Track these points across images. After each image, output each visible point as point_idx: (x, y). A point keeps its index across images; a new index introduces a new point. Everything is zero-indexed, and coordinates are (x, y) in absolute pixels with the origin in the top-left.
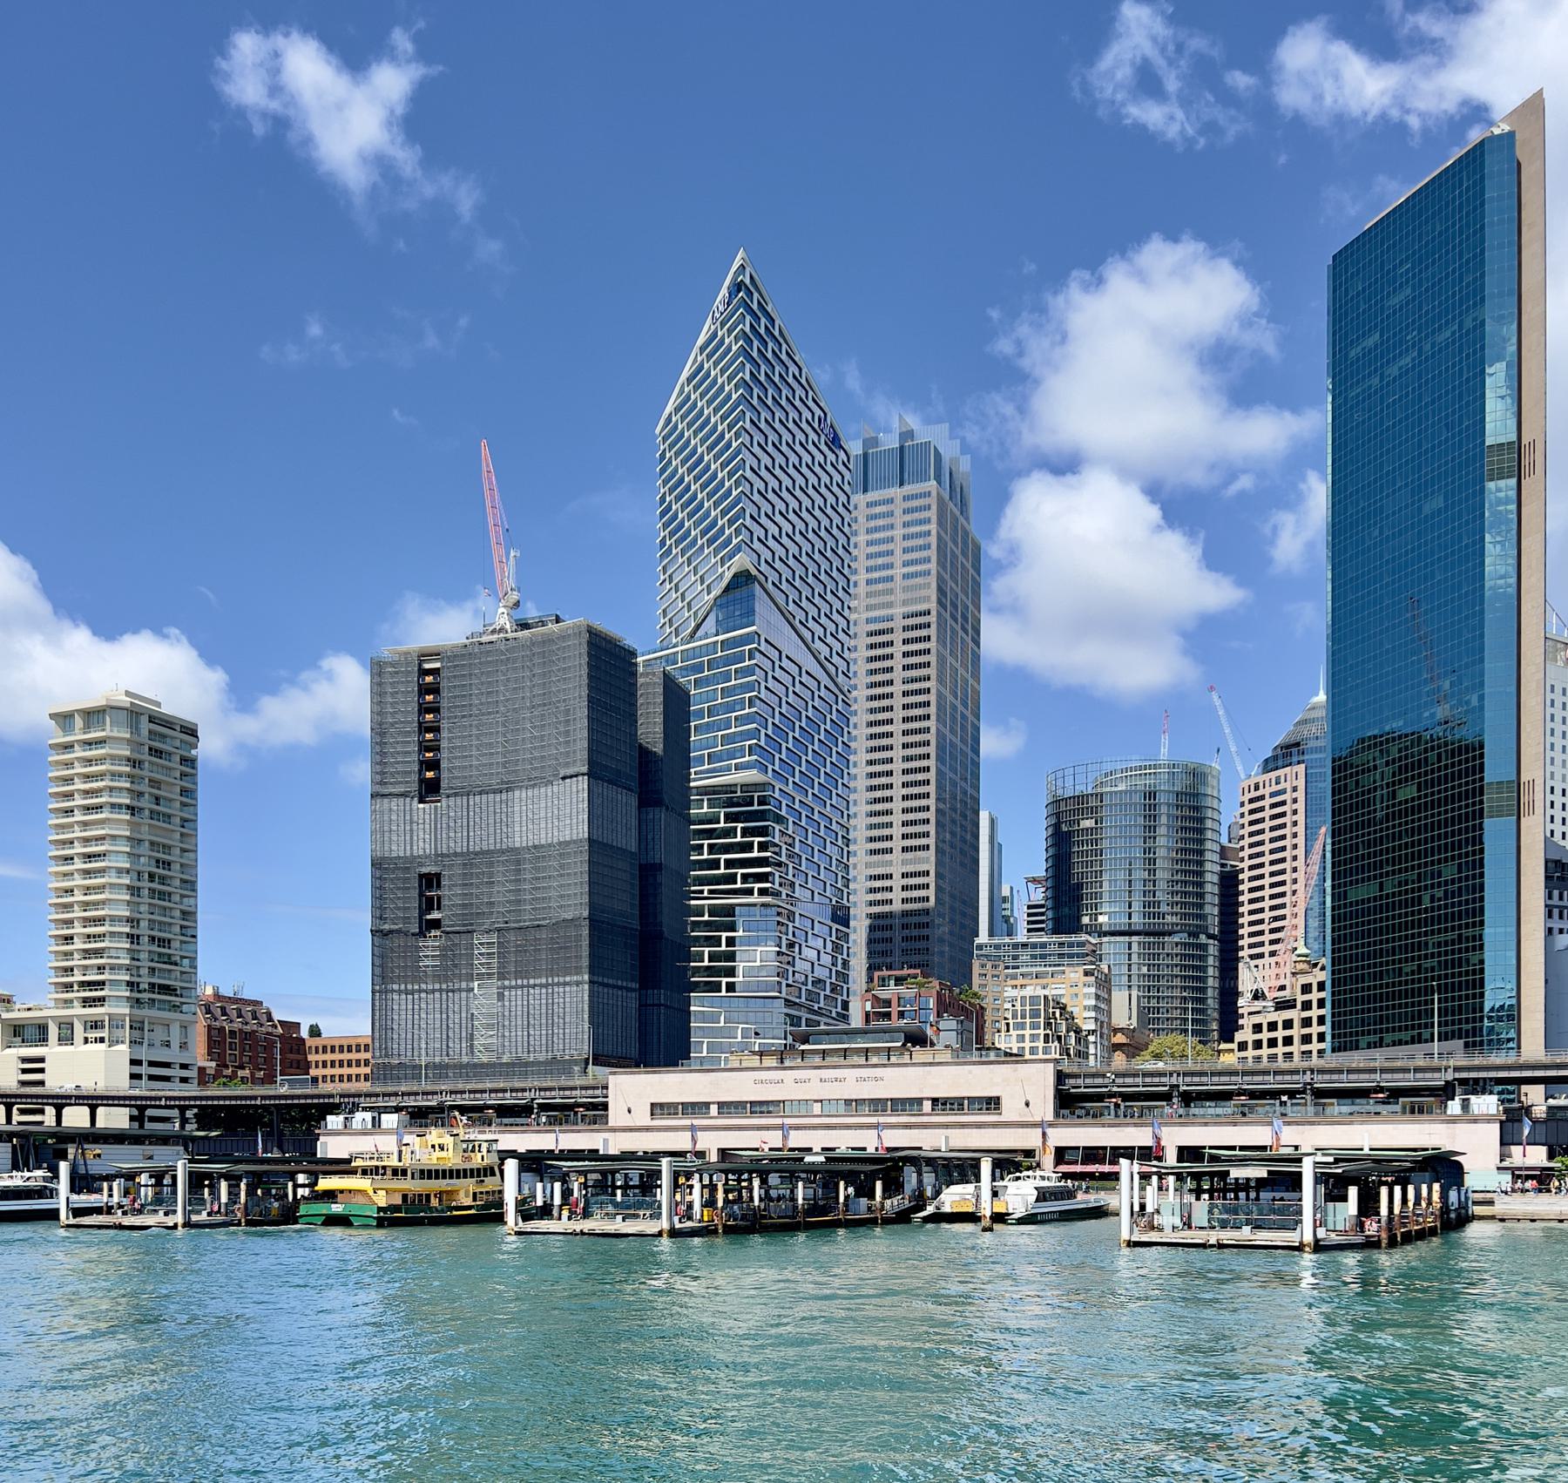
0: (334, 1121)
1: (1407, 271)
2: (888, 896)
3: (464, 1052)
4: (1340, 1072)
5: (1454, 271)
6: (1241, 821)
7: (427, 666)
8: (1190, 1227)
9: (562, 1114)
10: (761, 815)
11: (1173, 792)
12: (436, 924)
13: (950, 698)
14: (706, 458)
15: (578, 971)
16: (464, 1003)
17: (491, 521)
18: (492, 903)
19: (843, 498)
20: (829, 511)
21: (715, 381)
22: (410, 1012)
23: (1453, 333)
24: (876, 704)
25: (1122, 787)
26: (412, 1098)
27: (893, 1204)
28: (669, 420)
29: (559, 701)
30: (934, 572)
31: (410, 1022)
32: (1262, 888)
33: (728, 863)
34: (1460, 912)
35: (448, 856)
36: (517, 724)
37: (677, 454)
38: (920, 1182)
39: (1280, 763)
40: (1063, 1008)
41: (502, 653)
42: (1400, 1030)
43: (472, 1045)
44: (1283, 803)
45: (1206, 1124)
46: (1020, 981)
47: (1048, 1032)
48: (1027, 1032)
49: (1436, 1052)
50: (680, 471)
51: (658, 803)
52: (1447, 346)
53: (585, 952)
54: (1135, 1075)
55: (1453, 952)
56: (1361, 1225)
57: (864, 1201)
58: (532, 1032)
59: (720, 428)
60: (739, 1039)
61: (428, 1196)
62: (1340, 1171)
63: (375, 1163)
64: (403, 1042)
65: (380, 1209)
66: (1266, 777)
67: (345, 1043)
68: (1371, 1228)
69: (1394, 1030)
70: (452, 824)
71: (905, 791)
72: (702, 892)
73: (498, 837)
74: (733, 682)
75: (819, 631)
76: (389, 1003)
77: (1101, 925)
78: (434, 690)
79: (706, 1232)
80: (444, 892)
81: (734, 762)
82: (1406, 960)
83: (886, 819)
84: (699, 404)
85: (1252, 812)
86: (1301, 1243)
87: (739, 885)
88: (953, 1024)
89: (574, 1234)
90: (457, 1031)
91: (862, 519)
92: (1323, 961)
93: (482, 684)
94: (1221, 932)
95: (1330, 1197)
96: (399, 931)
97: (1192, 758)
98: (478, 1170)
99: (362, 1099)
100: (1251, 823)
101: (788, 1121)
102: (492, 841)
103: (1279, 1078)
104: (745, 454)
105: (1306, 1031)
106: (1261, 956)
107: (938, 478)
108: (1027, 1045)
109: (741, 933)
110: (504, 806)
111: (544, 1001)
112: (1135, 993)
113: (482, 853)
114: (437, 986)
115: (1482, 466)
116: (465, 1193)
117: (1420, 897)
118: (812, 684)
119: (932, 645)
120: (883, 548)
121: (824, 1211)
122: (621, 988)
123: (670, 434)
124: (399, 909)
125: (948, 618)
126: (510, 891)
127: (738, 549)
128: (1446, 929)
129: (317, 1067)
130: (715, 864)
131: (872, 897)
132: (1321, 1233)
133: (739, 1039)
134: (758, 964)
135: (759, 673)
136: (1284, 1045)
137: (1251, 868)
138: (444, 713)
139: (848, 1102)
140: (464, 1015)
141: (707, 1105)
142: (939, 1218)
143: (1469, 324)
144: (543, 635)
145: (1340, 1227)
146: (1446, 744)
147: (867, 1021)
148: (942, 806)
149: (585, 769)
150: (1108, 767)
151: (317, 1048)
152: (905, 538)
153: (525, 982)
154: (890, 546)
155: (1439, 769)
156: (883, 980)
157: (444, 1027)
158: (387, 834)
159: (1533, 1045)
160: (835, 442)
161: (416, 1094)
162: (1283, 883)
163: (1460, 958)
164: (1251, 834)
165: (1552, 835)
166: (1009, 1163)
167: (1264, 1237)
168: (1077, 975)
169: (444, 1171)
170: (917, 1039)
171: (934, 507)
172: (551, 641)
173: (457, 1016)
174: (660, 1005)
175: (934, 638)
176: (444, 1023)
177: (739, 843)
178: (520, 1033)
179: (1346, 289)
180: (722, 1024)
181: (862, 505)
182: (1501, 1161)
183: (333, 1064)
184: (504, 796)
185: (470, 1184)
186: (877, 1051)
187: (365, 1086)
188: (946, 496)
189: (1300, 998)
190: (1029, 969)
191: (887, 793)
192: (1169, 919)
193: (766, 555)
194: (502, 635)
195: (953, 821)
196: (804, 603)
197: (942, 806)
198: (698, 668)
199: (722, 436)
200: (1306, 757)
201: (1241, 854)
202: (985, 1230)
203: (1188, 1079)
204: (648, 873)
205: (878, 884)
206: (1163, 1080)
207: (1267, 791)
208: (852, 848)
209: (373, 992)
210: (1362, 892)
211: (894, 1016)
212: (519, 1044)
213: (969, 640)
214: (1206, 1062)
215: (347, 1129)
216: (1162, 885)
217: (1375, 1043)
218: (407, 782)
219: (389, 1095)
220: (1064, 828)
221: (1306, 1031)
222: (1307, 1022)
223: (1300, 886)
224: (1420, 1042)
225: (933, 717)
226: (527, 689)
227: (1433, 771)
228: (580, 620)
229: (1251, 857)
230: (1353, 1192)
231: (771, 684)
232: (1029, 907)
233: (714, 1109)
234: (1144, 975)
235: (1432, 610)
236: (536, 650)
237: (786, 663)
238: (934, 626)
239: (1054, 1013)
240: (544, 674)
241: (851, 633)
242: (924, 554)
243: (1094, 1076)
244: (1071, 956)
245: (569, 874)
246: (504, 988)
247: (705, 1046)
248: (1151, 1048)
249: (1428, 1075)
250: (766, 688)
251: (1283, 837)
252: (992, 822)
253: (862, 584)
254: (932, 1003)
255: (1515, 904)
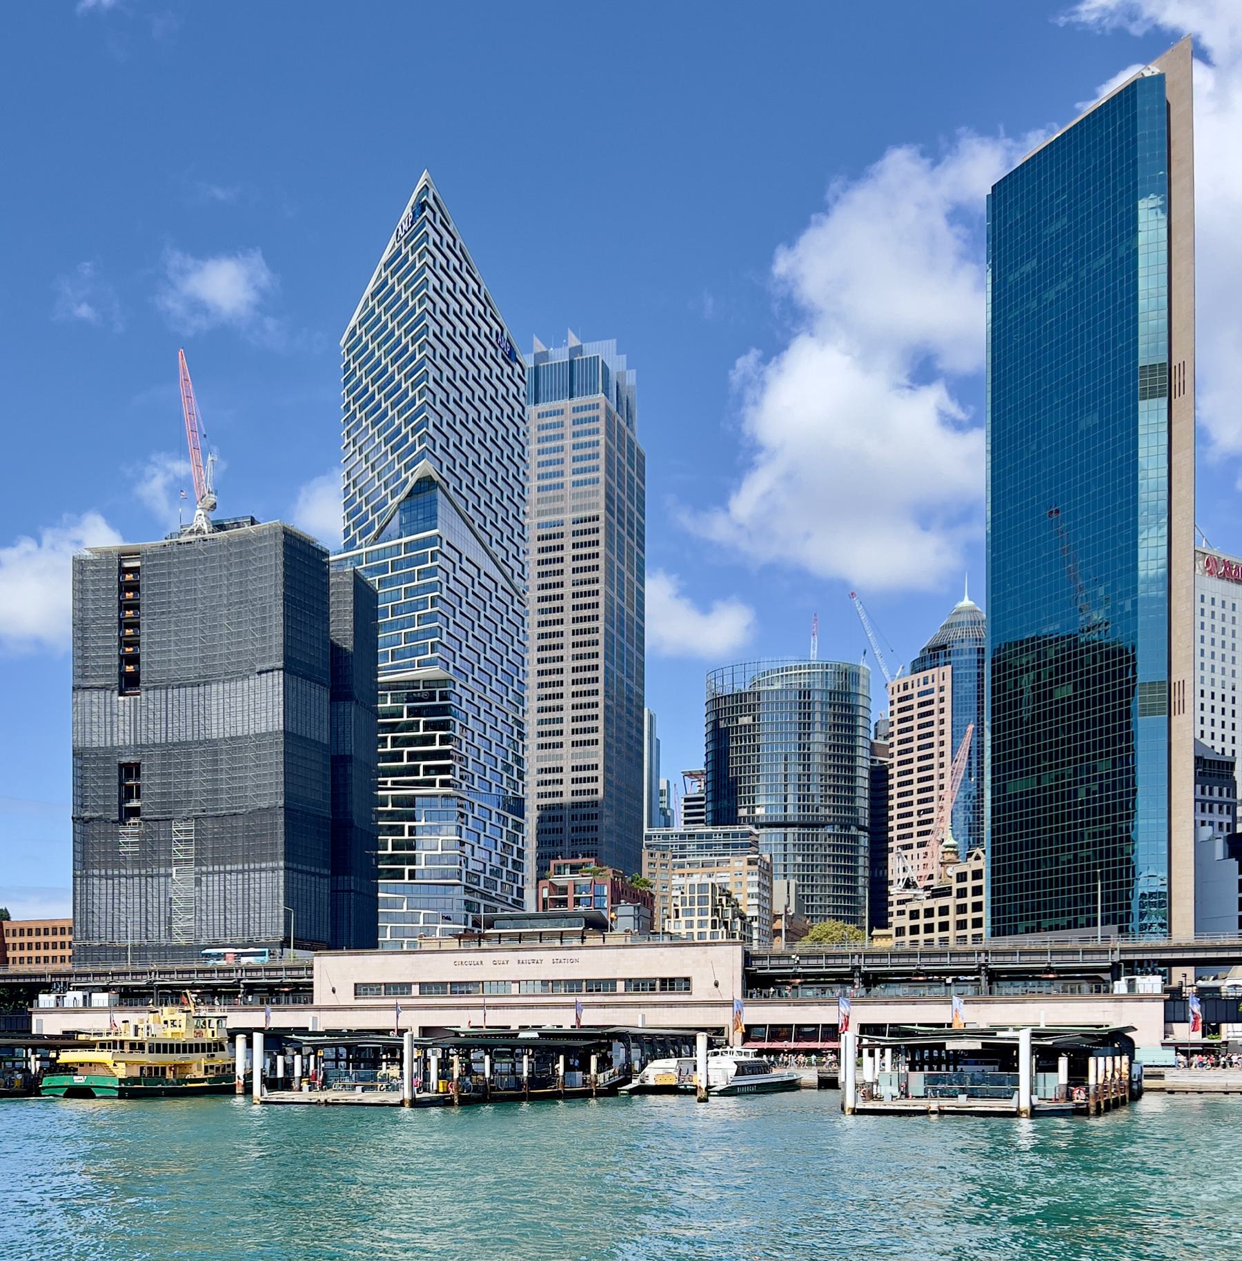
0: (45, 1000)
1: (1063, 202)
2: (558, 788)
3: (162, 934)
4: (1014, 954)
5: (1108, 202)
6: (891, 719)
7: (127, 565)
8: (907, 1096)
9: (270, 993)
10: (444, 710)
11: (826, 691)
12: (135, 812)
13: (617, 599)
14: (390, 370)
15: (273, 858)
16: (162, 888)
17: (188, 427)
18: (189, 793)
19: (518, 409)
20: (494, 422)
21: (399, 296)
22: (110, 897)
23: (1108, 261)
24: (546, 605)
25: (778, 686)
26: (122, 978)
27: (603, 1079)
28: (353, 333)
29: (255, 600)
30: (602, 480)
31: (110, 906)
32: (910, 782)
33: (412, 756)
34: (1114, 804)
35: (147, 746)
36: (214, 620)
37: (361, 366)
38: (628, 1056)
39: (928, 664)
40: (729, 895)
41: (200, 553)
42: (1057, 915)
43: (170, 929)
44: (931, 702)
45: (886, 1003)
46: (687, 870)
47: (715, 918)
48: (696, 918)
49: (1099, 935)
50: (364, 382)
51: (349, 697)
52: (1101, 273)
53: (281, 840)
54: (819, 957)
55: (1108, 842)
56: (1069, 1097)
57: (579, 1074)
58: (228, 916)
59: (404, 341)
60: (421, 924)
61: (164, 1069)
62: (1050, 1043)
63: (112, 1037)
64: (103, 925)
65: (121, 1081)
66: (915, 677)
67: (42, 926)
68: (1079, 1096)
69: (1051, 915)
70: (151, 716)
71: (575, 688)
72: (385, 783)
73: (196, 728)
74: (416, 583)
75: (496, 535)
76: (90, 888)
77: (758, 817)
78: (135, 587)
79: (443, 1102)
80: (144, 781)
81: (417, 659)
82: (1063, 850)
83: (556, 715)
84: (383, 318)
85: (901, 710)
86: (1018, 1108)
87: (421, 777)
88: (630, 910)
89: (318, 1103)
90: (156, 915)
91: (533, 429)
92: (978, 851)
93: (181, 582)
94: (871, 824)
95: (1040, 1069)
96: (99, 819)
97: (843, 657)
98: (209, 1045)
99: (73, 979)
100: (901, 721)
101: (489, 1001)
102: (189, 733)
103: (955, 959)
104: (428, 366)
105: (961, 917)
106: (909, 847)
107: (606, 391)
108: (696, 930)
109: (423, 823)
110: (201, 698)
111: (240, 887)
112: (793, 882)
113: (180, 743)
114: (136, 872)
115: (1136, 386)
116: (197, 1067)
117: (1076, 791)
118: (491, 586)
119: (601, 549)
120: (554, 456)
121: (544, 1083)
122: (314, 874)
123: (354, 346)
124: (99, 797)
125: (616, 524)
126: (207, 781)
127: (421, 456)
128: (1101, 821)
129: (14, 949)
130: (398, 757)
131: (542, 789)
132: (1035, 1102)
133: (421, 924)
134: (439, 852)
135: (441, 576)
136: (974, 927)
137: (900, 763)
138: (143, 610)
139: (544, 983)
140: (162, 899)
141: (409, 985)
142: (644, 1090)
143: (1122, 252)
144: (239, 536)
145: (1050, 1095)
146: (1101, 646)
147: (544, 908)
148: (610, 703)
149: (280, 664)
150: (765, 667)
151: (14, 931)
152: (575, 447)
153: (222, 868)
154: (561, 455)
155: (1094, 670)
156: (559, 868)
157: (143, 910)
158: (88, 726)
159: (1183, 929)
160: (511, 356)
161: (126, 974)
162: (931, 778)
163: (1114, 848)
164: (901, 732)
165: (1202, 736)
166: (716, 1039)
167: (980, 1105)
168: (741, 864)
169: (178, 1045)
170: (598, 925)
171: (603, 419)
172: (248, 542)
173: (156, 900)
174: (350, 891)
175: (602, 543)
176: (143, 906)
177: (422, 737)
178: (216, 917)
179: (1005, 218)
180: (405, 910)
181: (534, 416)
182: (1165, 1037)
183: (30, 946)
184: (201, 690)
185: (201, 1059)
186: (552, 935)
187: (66, 967)
188: (613, 408)
189: (956, 886)
190: (696, 859)
191: (558, 690)
192: (822, 812)
193: (447, 462)
194: (199, 536)
195: (620, 717)
196: (483, 508)
197: (610, 703)
198: (383, 569)
199: (406, 348)
200: (952, 659)
201: (891, 750)
202: (700, 1101)
203: (869, 961)
204: (339, 764)
205: (549, 777)
206: (845, 961)
207: (915, 691)
208: (526, 742)
209: (75, 877)
210: (1016, 787)
211: (571, 902)
212: (216, 927)
213: (634, 545)
214: (866, 945)
215: (59, 1008)
216: (816, 780)
217: (1033, 928)
218: (108, 676)
219: (100, 975)
220: (722, 725)
221: (961, 917)
222: (962, 909)
223: (947, 781)
224: (1076, 927)
225: (602, 618)
226: (224, 588)
227: (1088, 672)
228: (276, 522)
229: (900, 753)
230: (1063, 1063)
231: (452, 584)
232: (686, 800)
233: (415, 990)
234: (799, 865)
235: (1088, 520)
236: (233, 550)
237: (466, 565)
238: (602, 532)
239: (720, 900)
240: (241, 574)
241: (525, 537)
242: (593, 463)
243: (779, 957)
244: (735, 846)
245: (264, 765)
246: (202, 873)
247: (388, 930)
248: (811, 933)
249: (1096, 957)
250: (448, 588)
251: (931, 735)
252: (651, 717)
253: (534, 490)
254: (606, 890)
255: (1166, 797)
